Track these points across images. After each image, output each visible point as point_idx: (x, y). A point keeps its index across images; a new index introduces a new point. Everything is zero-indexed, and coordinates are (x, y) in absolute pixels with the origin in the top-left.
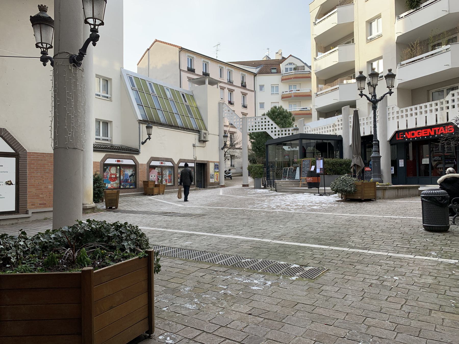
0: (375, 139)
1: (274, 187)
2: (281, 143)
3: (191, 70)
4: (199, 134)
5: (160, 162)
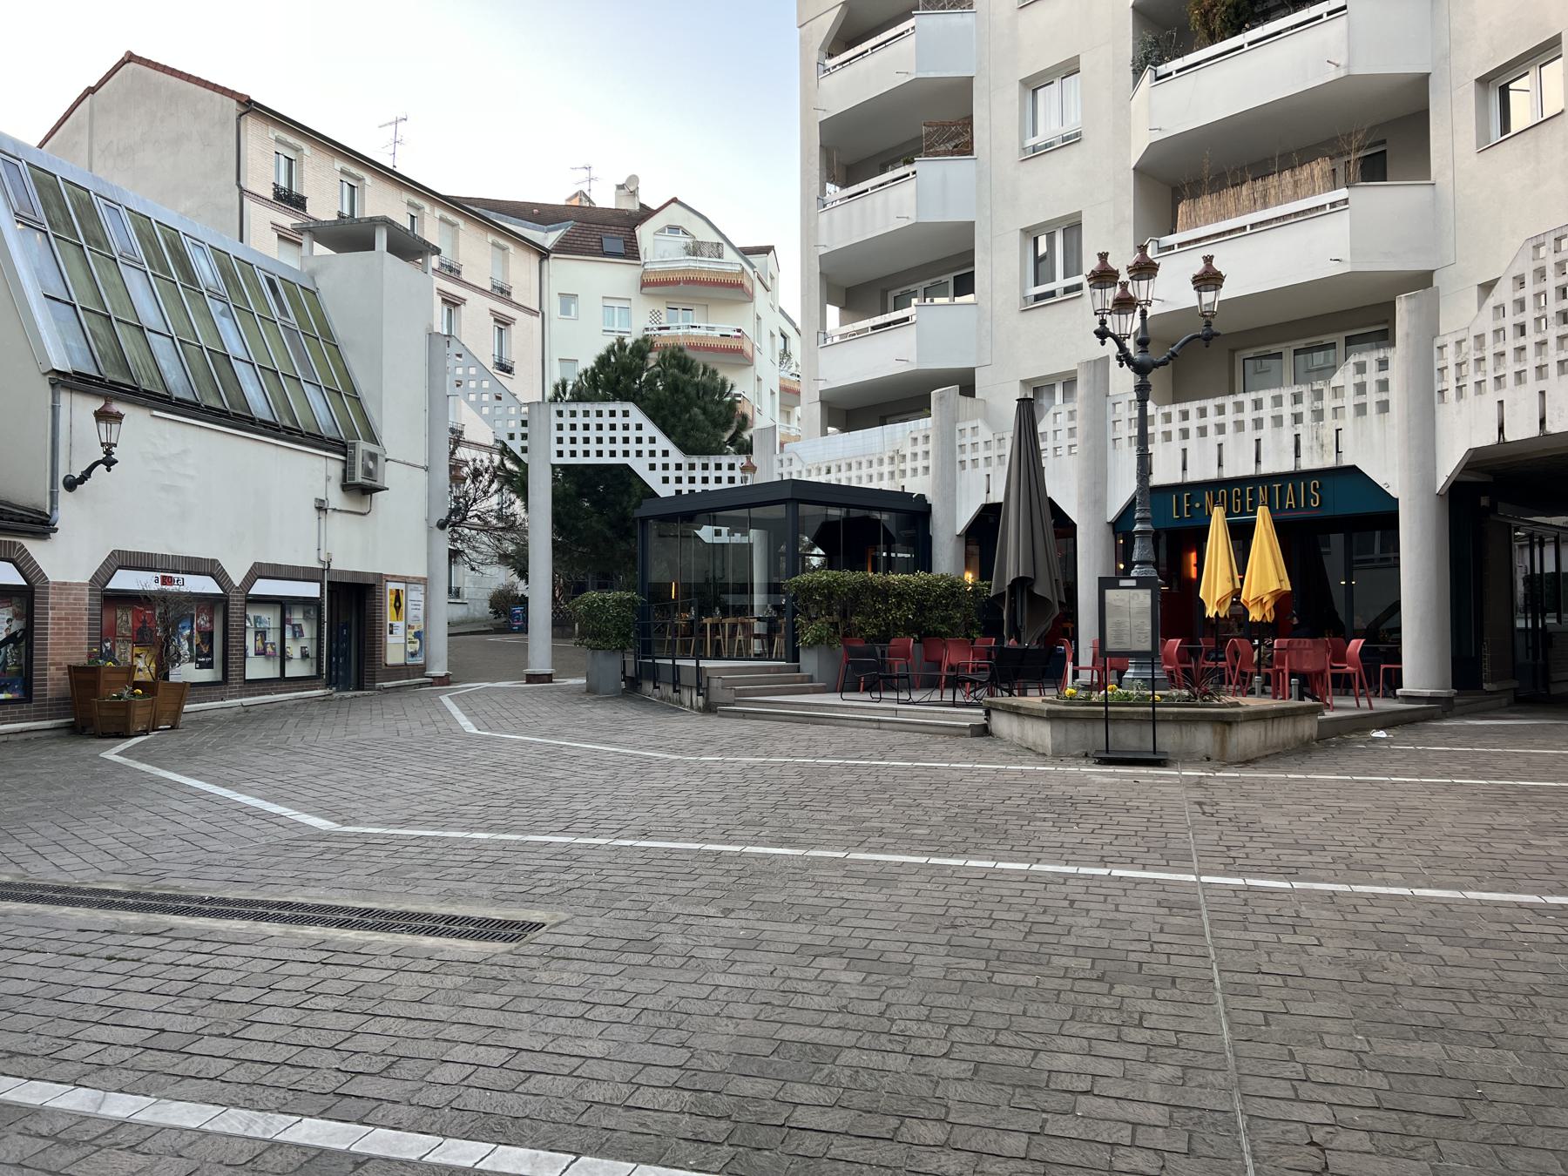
0: (1143, 515)
1: (698, 694)
2: (692, 511)
3: (290, 199)
4: (342, 458)
5: (159, 575)
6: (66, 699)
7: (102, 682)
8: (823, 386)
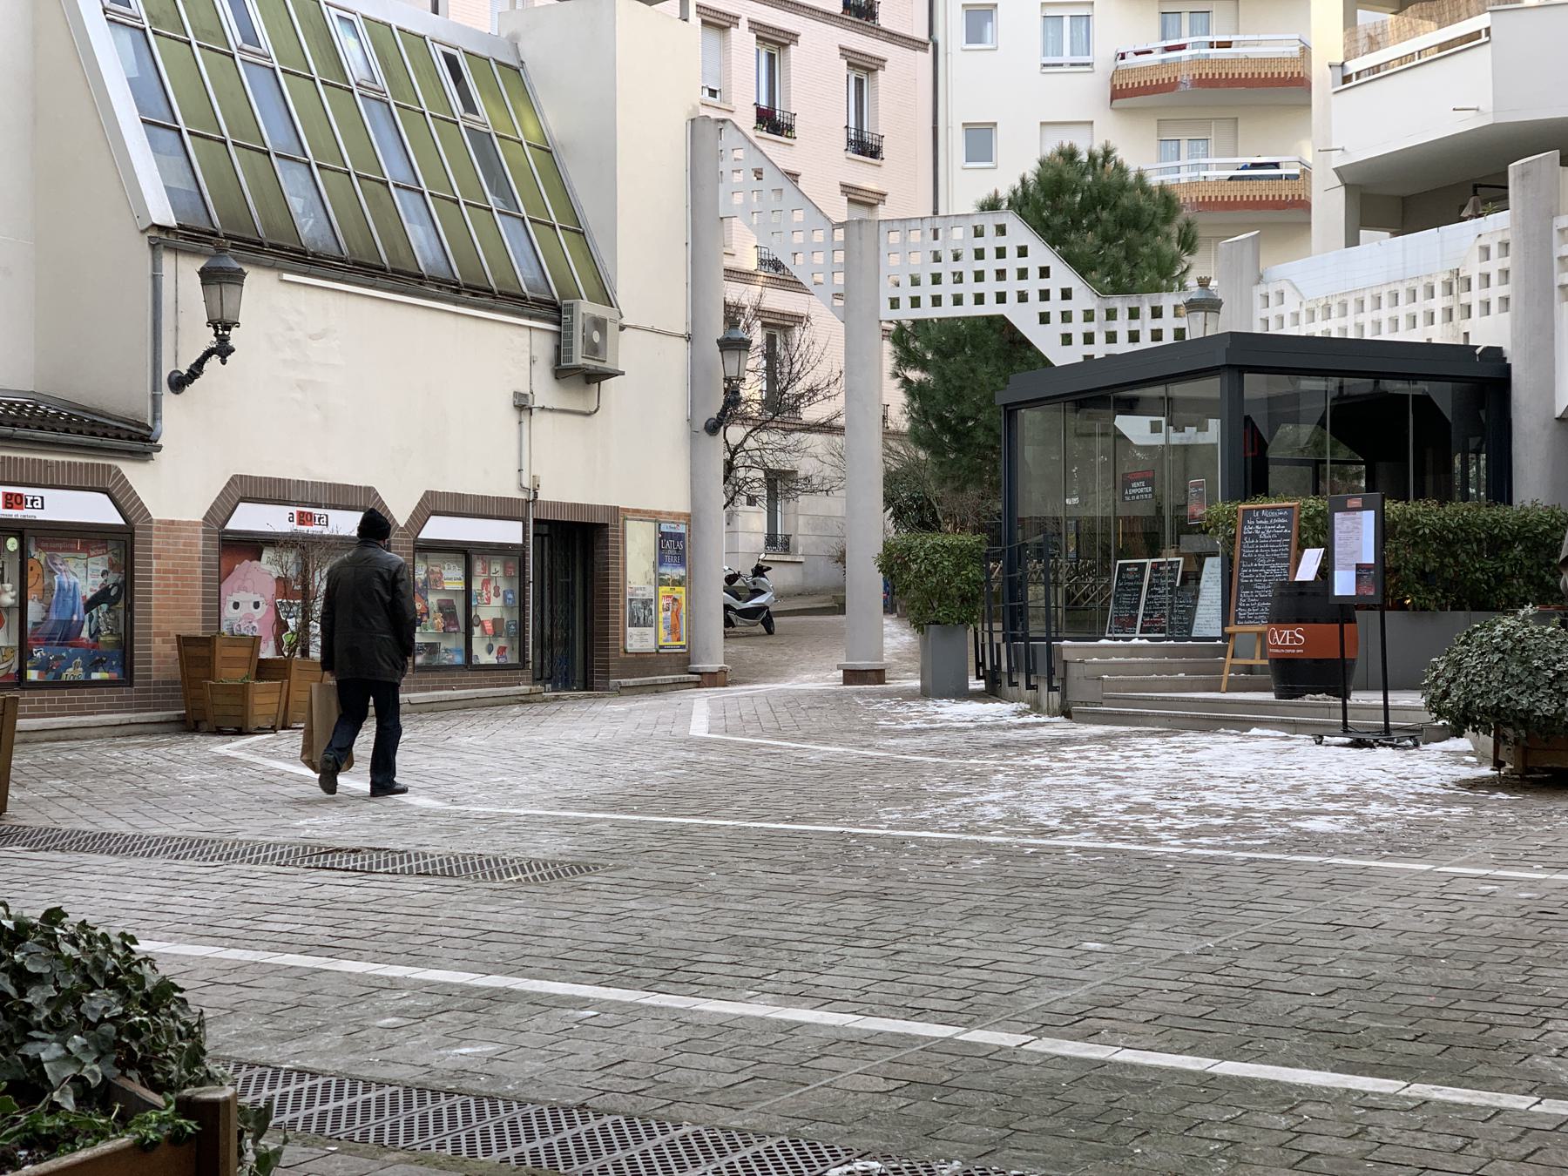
5: (295, 510)
6: (175, 683)
7: (218, 658)
8: (1339, 160)
